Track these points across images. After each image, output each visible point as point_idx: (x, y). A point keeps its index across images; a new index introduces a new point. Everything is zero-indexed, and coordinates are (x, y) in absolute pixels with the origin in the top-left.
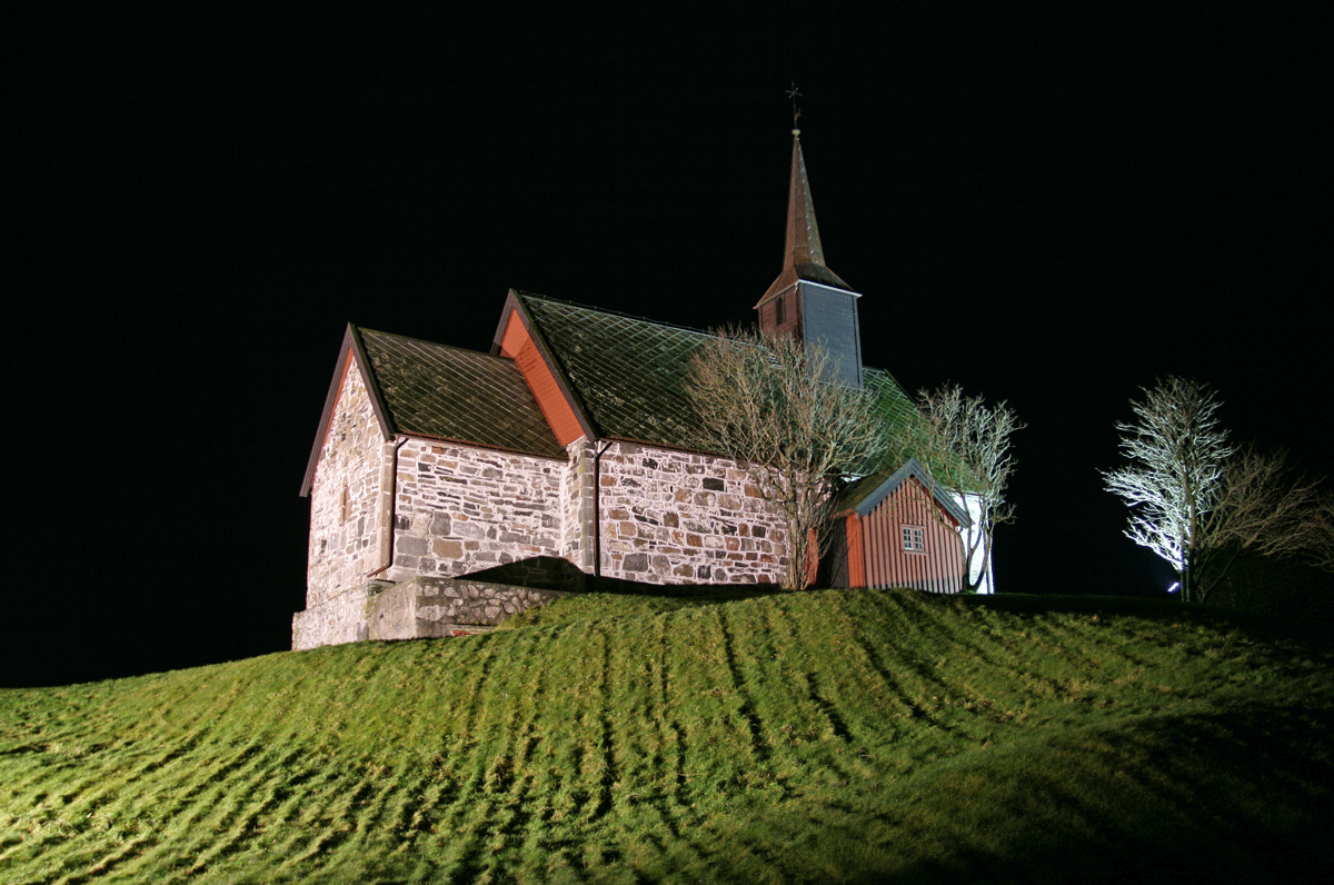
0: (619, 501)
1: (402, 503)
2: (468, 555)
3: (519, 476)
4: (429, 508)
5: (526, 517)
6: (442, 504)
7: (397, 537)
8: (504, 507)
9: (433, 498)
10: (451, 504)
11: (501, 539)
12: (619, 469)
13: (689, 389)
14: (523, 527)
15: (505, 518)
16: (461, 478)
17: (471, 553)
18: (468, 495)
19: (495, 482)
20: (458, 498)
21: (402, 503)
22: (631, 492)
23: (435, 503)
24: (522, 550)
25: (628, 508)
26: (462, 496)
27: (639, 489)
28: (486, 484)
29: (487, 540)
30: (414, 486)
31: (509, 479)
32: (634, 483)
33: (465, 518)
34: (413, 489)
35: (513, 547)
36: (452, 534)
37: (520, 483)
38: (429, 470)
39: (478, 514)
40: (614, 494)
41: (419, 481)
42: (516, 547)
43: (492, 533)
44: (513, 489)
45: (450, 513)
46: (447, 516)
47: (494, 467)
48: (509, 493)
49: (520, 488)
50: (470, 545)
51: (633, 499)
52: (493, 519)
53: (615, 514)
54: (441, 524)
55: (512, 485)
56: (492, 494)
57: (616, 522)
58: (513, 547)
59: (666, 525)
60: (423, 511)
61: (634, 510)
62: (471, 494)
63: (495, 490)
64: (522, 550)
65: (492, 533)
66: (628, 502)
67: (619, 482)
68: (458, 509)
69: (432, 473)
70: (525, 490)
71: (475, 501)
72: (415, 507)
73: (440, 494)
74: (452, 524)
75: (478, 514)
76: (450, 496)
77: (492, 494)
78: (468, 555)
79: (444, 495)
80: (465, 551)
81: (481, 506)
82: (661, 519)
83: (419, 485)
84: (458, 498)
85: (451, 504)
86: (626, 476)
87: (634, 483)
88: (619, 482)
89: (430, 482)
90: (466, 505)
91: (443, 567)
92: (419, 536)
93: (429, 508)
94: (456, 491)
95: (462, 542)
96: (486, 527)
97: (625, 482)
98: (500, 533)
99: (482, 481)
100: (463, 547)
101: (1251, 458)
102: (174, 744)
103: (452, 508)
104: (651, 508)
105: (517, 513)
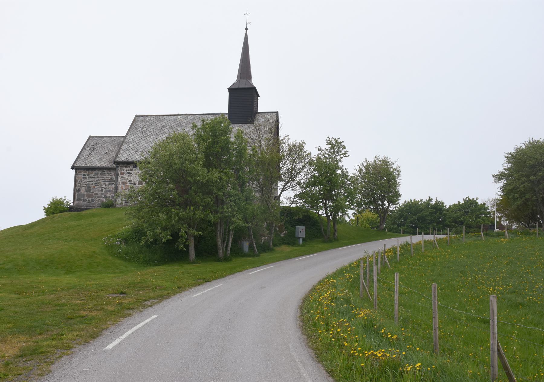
0: (125, 179)
1: (78, 185)
2: (95, 197)
3: (110, 174)
4: (85, 186)
5: (112, 185)
6: (88, 184)
7: (77, 194)
8: (106, 183)
9: (86, 183)
10: (91, 184)
11: (104, 192)
12: (125, 169)
13: (318, 224)
14: (111, 188)
15: (106, 186)
16: (94, 176)
17: (96, 196)
18: (95, 181)
19: (103, 176)
20: (93, 182)
21: (78, 185)
22: (129, 176)
23: (87, 184)
24: (110, 194)
25: (127, 181)
26: (94, 181)
27: (131, 175)
28: (101, 177)
29: (100, 192)
30: (81, 180)
31: (107, 175)
32: (130, 173)
33: (95, 187)
34: (81, 181)
35: (108, 194)
36: (91, 192)
37: (110, 175)
38: (85, 175)
39: (98, 186)
40: (124, 177)
41: (83, 179)
42: (109, 193)
43: (102, 190)
44: (108, 178)
45: (90, 186)
46: (90, 187)
47: (103, 172)
48: (107, 179)
49: (110, 177)
50: (96, 194)
51: (129, 178)
52: (102, 186)
53: (123, 183)
54: (88, 189)
55: (108, 176)
56: (102, 180)
57: (123, 185)
58: (108, 194)
59: (138, 185)
60: (83, 186)
61: (129, 181)
62: (96, 180)
63: (103, 178)
64: (110, 194)
65: (102, 190)
66: (127, 179)
67: (125, 173)
68: (93, 185)
69: (86, 176)
70: (112, 177)
71: (98, 182)
72: (82, 185)
73: (88, 181)
74: (91, 189)
75: (98, 186)
76: (91, 182)
77: (102, 180)
78: (95, 197)
79: (89, 181)
80: (94, 196)
81: (99, 183)
82: (137, 183)
83: (83, 180)
84: (93, 182)
85: (91, 184)
86: (128, 171)
87: (130, 173)
88: (125, 173)
89: (86, 179)
90: (95, 183)
91: (89, 200)
92: (83, 193)
93: (85, 186)
94: (92, 180)
95: (94, 193)
96: (100, 189)
97: (127, 173)
98: (104, 190)
99: (100, 176)
100: (94, 195)
101: (248, 153)
102: (49, 242)
103: (91, 185)
104: (134, 180)
105: (109, 184)
